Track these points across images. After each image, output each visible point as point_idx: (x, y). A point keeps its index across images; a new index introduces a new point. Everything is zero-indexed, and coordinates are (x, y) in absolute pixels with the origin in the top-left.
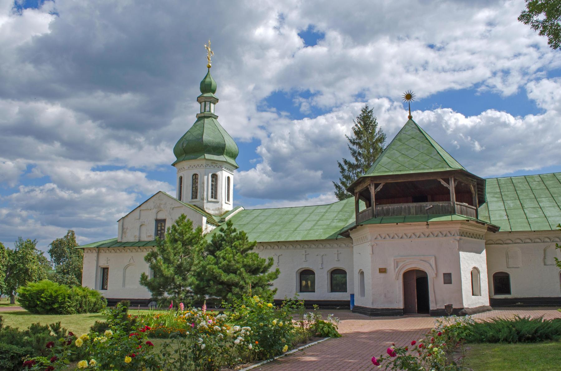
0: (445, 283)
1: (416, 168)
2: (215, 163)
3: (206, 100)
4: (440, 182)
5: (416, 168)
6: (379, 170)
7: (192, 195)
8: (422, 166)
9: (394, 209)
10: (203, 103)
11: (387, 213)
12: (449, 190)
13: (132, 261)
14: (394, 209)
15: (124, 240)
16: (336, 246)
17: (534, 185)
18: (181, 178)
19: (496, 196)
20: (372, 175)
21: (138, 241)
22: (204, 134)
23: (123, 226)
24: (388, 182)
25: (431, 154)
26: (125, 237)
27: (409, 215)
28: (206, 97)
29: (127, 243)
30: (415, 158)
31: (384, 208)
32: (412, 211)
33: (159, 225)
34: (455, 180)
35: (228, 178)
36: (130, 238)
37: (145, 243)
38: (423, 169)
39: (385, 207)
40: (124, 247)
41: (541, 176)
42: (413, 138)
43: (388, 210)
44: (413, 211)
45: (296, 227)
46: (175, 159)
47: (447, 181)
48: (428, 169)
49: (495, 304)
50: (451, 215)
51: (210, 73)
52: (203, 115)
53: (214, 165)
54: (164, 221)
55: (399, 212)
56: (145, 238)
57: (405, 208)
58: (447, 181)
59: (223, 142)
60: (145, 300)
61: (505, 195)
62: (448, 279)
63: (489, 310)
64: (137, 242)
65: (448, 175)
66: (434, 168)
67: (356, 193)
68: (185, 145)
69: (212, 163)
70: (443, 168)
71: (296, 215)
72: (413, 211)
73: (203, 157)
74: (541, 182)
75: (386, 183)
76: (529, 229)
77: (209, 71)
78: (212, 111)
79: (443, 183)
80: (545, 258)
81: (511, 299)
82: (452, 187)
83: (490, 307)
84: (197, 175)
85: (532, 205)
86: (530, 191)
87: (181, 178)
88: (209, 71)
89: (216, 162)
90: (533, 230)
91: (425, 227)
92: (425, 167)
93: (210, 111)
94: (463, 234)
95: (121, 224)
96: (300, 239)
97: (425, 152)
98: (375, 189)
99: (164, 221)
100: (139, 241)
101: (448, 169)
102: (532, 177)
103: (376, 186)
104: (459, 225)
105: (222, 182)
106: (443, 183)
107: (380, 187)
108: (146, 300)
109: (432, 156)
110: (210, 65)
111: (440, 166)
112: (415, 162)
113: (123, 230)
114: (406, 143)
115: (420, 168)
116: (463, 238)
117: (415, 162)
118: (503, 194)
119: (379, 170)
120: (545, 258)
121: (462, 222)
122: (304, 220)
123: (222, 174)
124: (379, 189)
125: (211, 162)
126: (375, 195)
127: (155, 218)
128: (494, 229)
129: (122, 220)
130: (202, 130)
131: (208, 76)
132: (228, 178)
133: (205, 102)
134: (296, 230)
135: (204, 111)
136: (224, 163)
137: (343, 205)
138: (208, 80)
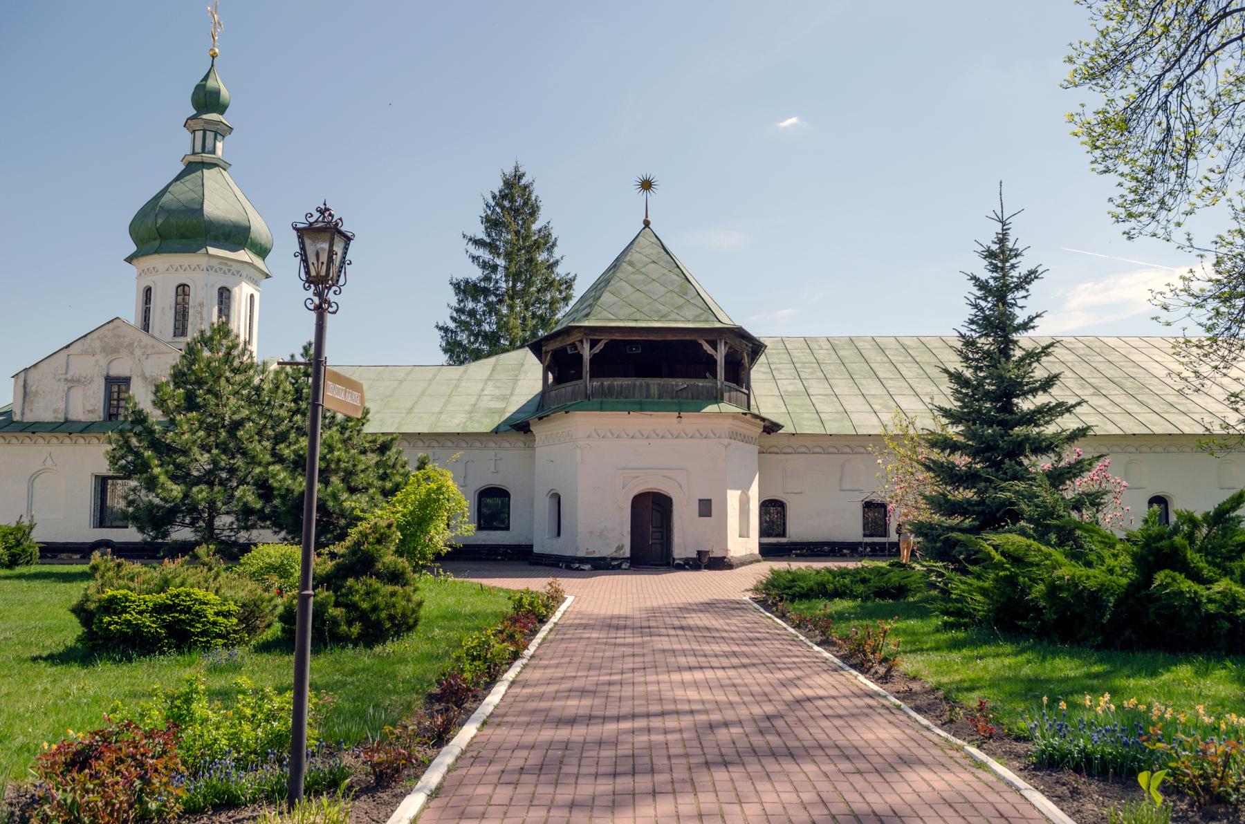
0: (700, 516)
1: (663, 317)
2: (226, 264)
3: (207, 127)
4: (701, 345)
5: (663, 317)
6: (599, 316)
7: (175, 328)
8: (673, 316)
9: (622, 385)
10: (199, 134)
11: (606, 393)
12: (715, 361)
13: (49, 462)
14: (622, 385)
15: (30, 417)
16: (493, 445)
17: (821, 355)
18: (148, 291)
19: (762, 369)
20: (586, 324)
21: (62, 421)
22: (206, 202)
23: (25, 387)
24: (614, 338)
25: (686, 294)
26: (31, 410)
27: (647, 397)
28: (208, 122)
29: (37, 425)
30: (660, 300)
31: (605, 383)
32: (652, 391)
33: (115, 389)
34: (726, 343)
35: (252, 296)
36: (43, 412)
37: (84, 426)
38: (675, 321)
39: (607, 382)
40: (34, 433)
41: (830, 339)
42: (654, 262)
43: (610, 387)
44: (654, 390)
45: (409, 405)
46: (133, 248)
47: (714, 345)
48: (683, 321)
49: (768, 552)
50: (717, 403)
51: (215, 68)
52: (197, 159)
53: (225, 268)
54: (126, 381)
55: (621, 393)
56: (79, 413)
57: (641, 385)
58: (714, 345)
59: (246, 223)
60: (83, 543)
61: (778, 369)
62: (705, 508)
63: (758, 561)
64: (63, 423)
65: (715, 335)
66: (694, 321)
67: (547, 352)
68: (160, 221)
69: (220, 264)
70: (706, 321)
71: (401, 382)
72: (654, 390)
73: (203, 250)
74: (832, 352)
75: (611, 340)
76: (820, 431)
77: (212, 65)
78: (219, 152)
79: (707, 347)
80: (841, 479)
81: (786, 544)
82: (720, 355)
83: (760, 557)
84: (186, 288)
85: (822, 391)
86: (816, 365)
87: (148, 291)
88: (212, 65)
89: (229, 263)
90: (829, 433)
91: (675, 420)
92: (678, 317)
93: (214, 152)
94: (734, 436)
95: (21, 383)
96: (426, 431)
97: (677, 290)
98: (591, 349)
99: (126, 381)
100: (67, 421)
101: (718, 325)
102: (815, 339)
103: (593, 344)
104: (730, 421)
105: (240, 305)
106: (707, 347)
107: (600, 346)
108: (86, 543)
109: (688, 298)
110: (217, 50)
111: (703, 318)
112: (661, 307)
113: (26, 393)
114: (643, 270)
115: (669, 318)
116: (732, 441)
117: (661, 307)
118: (772, 367)
119: (599, 316)
120: (841, 479)
121: (734, 416)
122: (423, 393)
123: (241, 289)
124: (597, 350)
125: (219, 261)
126: (591, 360)
127: (105, 373)
128: (771, 428)
129: (23, 374)
130: (201, 193)
131: (212, 74)
132: (252, 296)
133: (205, 131)
134: (410, 411)
135: (200, 150)
136: (245, 265)
137: (490, 368)
138: (211, 83)
